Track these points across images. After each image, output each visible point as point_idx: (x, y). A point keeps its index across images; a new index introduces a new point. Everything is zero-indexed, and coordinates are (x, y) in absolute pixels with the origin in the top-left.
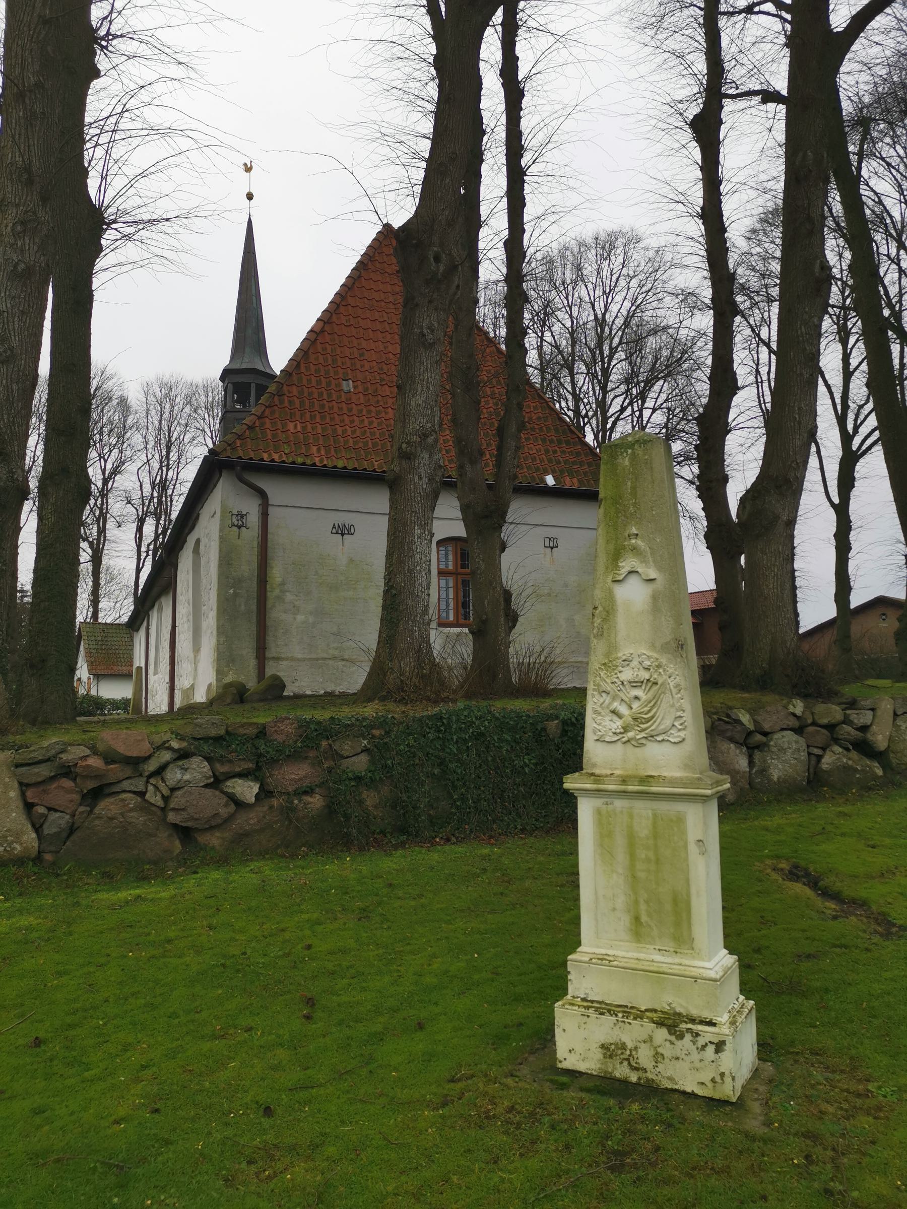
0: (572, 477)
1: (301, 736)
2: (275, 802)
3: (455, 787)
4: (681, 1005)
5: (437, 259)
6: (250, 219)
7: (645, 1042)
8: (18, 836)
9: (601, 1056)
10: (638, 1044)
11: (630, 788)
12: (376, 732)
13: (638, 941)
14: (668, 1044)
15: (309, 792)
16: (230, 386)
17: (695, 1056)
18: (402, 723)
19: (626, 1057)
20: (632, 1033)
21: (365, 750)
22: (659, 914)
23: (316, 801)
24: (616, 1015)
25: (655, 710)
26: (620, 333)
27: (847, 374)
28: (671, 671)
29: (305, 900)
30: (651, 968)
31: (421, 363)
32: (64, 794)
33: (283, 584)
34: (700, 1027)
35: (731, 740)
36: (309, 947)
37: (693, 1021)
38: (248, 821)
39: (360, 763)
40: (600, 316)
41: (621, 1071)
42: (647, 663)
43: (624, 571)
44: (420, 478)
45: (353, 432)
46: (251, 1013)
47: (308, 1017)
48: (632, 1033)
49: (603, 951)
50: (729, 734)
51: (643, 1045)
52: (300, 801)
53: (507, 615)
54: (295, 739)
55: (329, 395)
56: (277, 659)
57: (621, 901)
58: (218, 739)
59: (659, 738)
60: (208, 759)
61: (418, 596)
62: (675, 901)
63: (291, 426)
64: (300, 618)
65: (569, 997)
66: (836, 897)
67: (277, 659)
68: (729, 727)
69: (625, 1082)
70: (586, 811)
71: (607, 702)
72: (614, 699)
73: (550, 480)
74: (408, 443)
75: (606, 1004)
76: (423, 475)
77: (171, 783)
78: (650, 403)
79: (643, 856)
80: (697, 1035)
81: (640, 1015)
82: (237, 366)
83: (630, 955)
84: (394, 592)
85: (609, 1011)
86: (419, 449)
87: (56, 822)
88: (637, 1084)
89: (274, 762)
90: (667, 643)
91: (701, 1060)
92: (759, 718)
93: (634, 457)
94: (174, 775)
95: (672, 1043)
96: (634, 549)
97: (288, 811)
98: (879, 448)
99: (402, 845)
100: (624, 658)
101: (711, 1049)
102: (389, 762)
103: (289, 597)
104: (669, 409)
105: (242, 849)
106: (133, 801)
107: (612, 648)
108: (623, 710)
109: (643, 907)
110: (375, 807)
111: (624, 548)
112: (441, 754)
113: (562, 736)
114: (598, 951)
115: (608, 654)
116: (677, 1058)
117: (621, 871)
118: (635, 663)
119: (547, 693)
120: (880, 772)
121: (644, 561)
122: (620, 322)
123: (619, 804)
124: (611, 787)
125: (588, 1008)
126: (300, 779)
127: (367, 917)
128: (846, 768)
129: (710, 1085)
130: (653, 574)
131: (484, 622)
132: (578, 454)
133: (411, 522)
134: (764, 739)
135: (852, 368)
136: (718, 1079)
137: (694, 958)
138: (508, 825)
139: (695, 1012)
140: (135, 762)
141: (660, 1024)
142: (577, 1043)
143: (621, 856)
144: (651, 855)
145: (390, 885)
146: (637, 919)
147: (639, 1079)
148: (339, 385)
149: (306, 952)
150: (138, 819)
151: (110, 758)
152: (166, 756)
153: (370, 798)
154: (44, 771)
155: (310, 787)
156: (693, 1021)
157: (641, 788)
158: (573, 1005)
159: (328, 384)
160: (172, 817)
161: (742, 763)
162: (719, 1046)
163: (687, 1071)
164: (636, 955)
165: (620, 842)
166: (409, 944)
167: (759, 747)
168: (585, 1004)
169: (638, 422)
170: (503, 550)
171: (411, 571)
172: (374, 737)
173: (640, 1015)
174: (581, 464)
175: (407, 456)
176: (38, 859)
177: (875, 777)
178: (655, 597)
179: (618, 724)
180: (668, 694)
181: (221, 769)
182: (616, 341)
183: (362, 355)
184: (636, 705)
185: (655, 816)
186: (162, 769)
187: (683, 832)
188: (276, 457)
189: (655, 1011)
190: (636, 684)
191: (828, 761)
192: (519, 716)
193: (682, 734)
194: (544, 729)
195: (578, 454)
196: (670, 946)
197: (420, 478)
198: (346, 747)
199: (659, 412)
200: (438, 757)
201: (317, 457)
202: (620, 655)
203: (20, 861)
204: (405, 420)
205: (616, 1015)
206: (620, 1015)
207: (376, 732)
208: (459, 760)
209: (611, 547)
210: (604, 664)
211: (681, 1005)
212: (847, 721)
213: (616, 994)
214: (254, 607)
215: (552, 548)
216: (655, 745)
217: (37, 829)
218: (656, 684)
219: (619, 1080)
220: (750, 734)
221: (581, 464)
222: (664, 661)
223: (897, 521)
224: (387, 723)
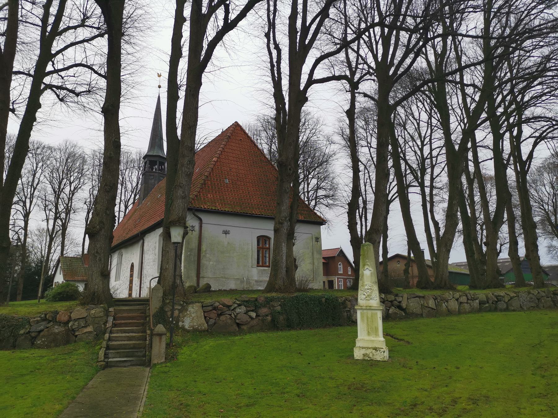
2: (260, 318)
4: (377, 346)
5: (290, 169)
6: (159, 97)
8: (204, 324)
15: (267, 316)
16: (148, 162)
20: (368, 352)
22: (372, 331)
23: (269, 318)
32: (213, 314)
33: (206, 251)
38: (254, 322)
39: (278, 308)
41: (367, 358)
45: (230, 198)
55: (221, 184)
56: (203, 277)
57: (365, 329)
58: (247, 301)
60: (245, 306)
63: (209, 195)
64: (211, 263)
66: (397, 339)
67: (203, 277)
70: (359, 313)
77: (237, 312)
81: (370, 348)
82: (151, 154)
87: (212, 321)
89: (260, 307)
94: (238, 310)
97: (263, 321)
98: (398, 199)
103: (208, 255)
105: (252, 330)
106: (228, 316)
107: (363, 282)
120: (404, 314)
123: (365, 311)
128: (395, 313)
140: (228, 307)
142: (358, 354)
143: (366, 321)
148: (223, 181)
150: (229, 321)
151: (224, 305)
152: (236, 305)
153: (281, 318)
154: (210, 308)
157: (369, 308)
159: (220, 180)
160: (237, 321)
162: (384, 352)
163: (379, 356)
165: (365, 318)
173: (370, 348)
175: (282, 224)
176: (207, 331)
177: (403, 316)
178: (371, 273)
179: (365, 297)
181: (249, 309)
183: (230, 170)
186: (235, 308)
188: (206, 207)
191: (391, 311)
196: (375, 336)
198: (275, 304)
201: (219, 207)
203: (204, 331)
212: (395, 300)
214: (196, 259)
217: (207, 323)
223: (404, 228)
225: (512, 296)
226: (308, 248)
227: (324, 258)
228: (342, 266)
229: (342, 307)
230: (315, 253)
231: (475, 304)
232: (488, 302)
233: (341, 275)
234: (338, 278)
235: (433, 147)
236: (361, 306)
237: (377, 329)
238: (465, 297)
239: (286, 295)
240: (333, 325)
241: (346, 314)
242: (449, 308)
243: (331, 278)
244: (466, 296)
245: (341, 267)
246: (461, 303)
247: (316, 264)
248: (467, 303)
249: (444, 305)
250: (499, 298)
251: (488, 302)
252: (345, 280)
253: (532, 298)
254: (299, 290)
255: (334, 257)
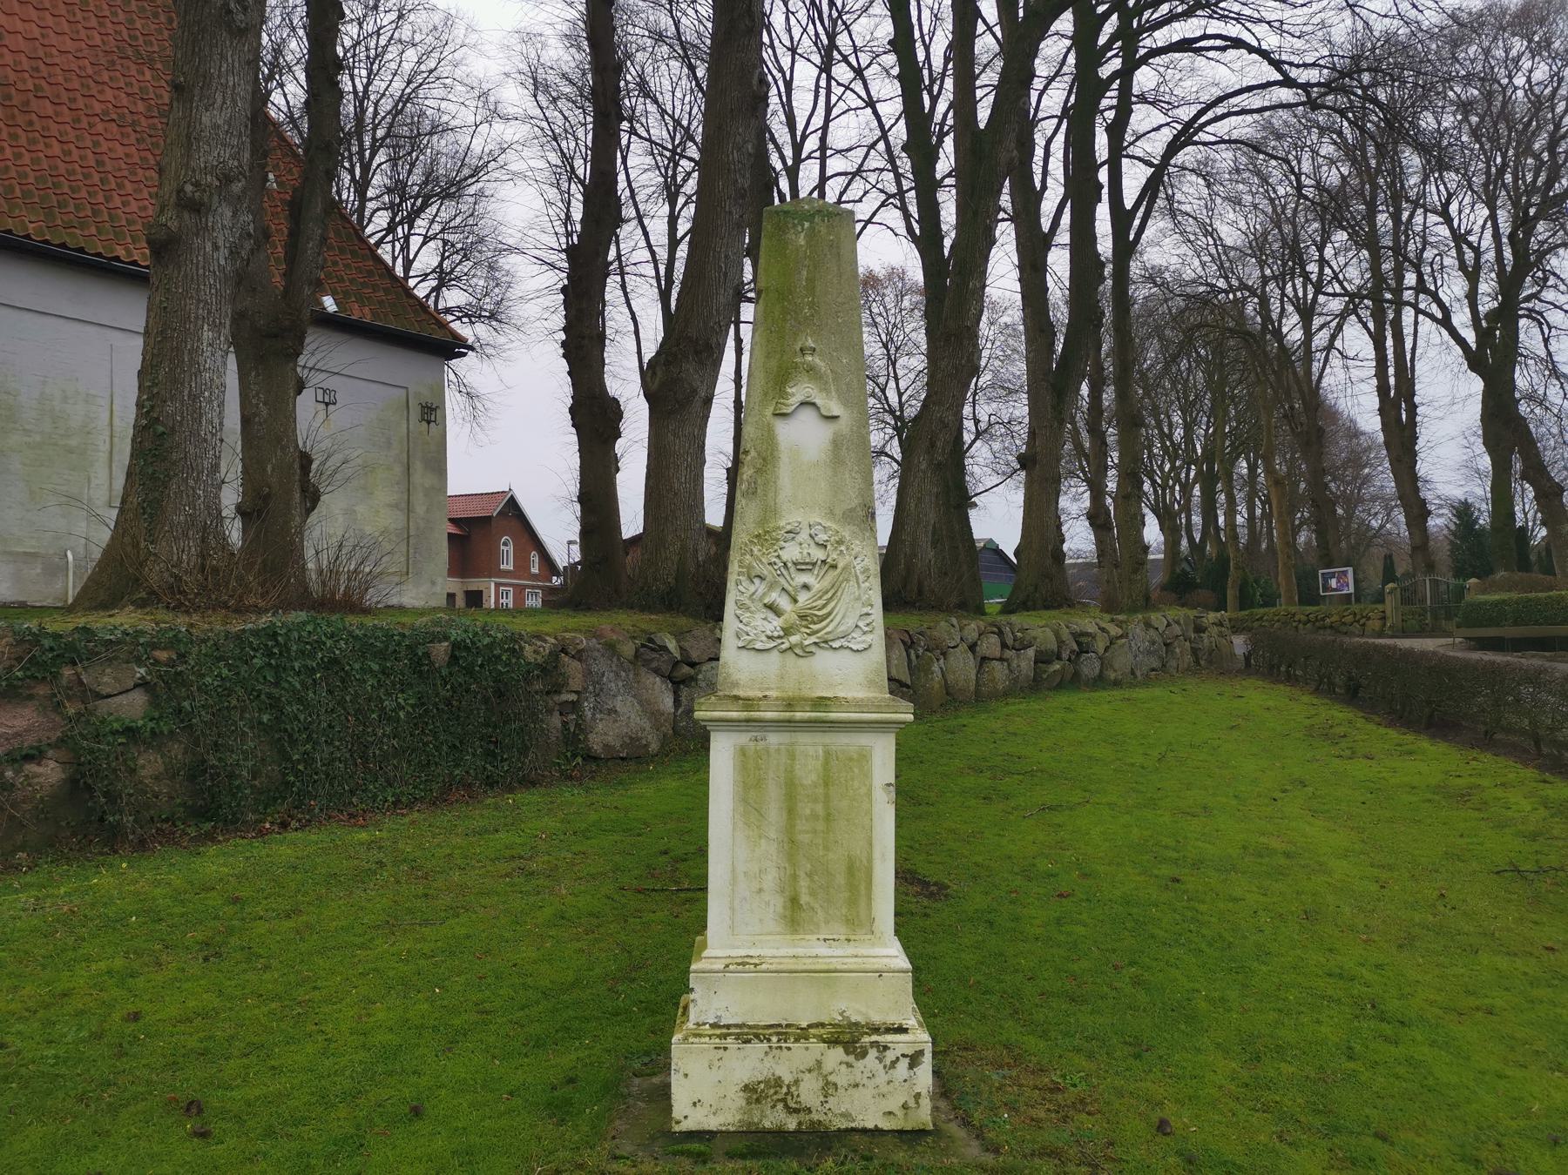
0: (362, 306)
1: (19, 659)
3: (293, 742)
4: (859, 1010)
7: (810, 1071)
9: (744, 1103)
10: (801, 1075)
11: (799, 715)
12: (163, 655)
13: (795, 932)
14: (844, 1067)
15: (35, 756)
17: (882, 1078)
18: (204, 641)
19: (780, 1097)
20: (790, 1063)
21: (142, 684)
23: (49, 773)
24: (769, 1040)
25: (832, 604)
26: (388, 119)
27: (674, 243)
28: (857, 549)
29: (84, 940)
30: (818, 967)
31: (223, 57)
34: (889, 1037)
35: (657, 671)
36: (136, 1017)
37: (876, 1030)
39: (132, 706)
40: (360, 88)
41: (774, 1118)
42: (822, 537)
43: (794, 401)
44: (216, 247)
46: (79, 1147)
47: (203, 1135)
48: (790, 1063)
49: (743, 952)
50: (654, 665)
51: (807, 1076)
52: (17, 772)
53: (304, 491)
54: (7, 663)
57: (770, 880)
59: (836, 644)
61: (205, 440)
62: (851, 870)
65: (690, 1025)
68: (655, 655)
69: (779, 1133)
70: (723, 753)
71: (760, 591)
72: (771, 587)
73: (329, 304)
74: (197, 185)
75: (750, 1027)
76: (221, 243)
78: (421, 224)
79: (808, 812)
80: (886, 1048)
81: (802, 1034)
83: (782, 952)
84: (161, 429)
85: (757, 1036)
86: (216, 198)
88: (798, 1132)
90: (851, 510)
91: (889, 1082)
92: (686, 645)
93: (812, 234)
95: (849, 1065)
96: (811, 370)
99: (210, 837)
100: (789, 528)
101: (904, 1063)
102: (186, 704)
104: (445, 242)
108: (784, 603)
109: (804, 883)
110: (157, 778)
111: (796, 366)
112: (274, 691)
113: (449, 665)
114: (734, 953)
115: (763, 521)
116: (856, 1086)
117: (773, 835)
118: (803, 536)
119: (366, 611)
121: (825, 389)
122: (386, 104)
123: (774, 739)
124: (769, 715)
125: (725, 1036)
126: (17, 735)
127: (218, 955)
129: (900, 1113)
130: (835, 408)
131: (266, 498)
132: (370, 274)
133: (197, 318)
134: (692, 671)
135: (679, 235)
136: (912, 1103)
137: (873, 945)
138: (375, 797)
139: (877, 1018)
141: (832, 1042)
142: (705, 1089)
144: (819, 808)
145: (236, 900)
146: (794, 901)
147: (800, 1123)
149: (131, 1027)
153: (149, 764)
155: (38, 748)
156: (876, 1030)
157: (814, 716)
158: (700, 1036)
161: (667, 702)
164: (791, 952)
165: (774, 794)
166: (315, 988)
167: (689, 681)
168: (718, 1032)
169: (402, 249)
170: (300, 393)
171: (194, 397)
172: (157, 662)
173: (802, 1034)
174: (375, 288)
175: (196, 208)
178: (836, 443)
179: (774, 625)
180: (853, 583)
182: (380, 133)
184: (803, 597)
185: (827, 754)
187: (867, 775)
189: (822, 1025)
190: (804, 566)
192: (389, 636)
193: (868, 638)
194: (427, 655)
195: (370, 274)
196: (840, 931)
197: (216, 247)
198: (107, 680)
199: (432, 244)
200: (269, 696)
202: (782, 523)
204: (190, 144)
205: (769, 1040)
206: (774, 1039)
207: (163, 655)
208: (300, 701)
209: (774, 363)
210: (758, 536)
211: (860, 1012)
213: (763, 1009)
215: (327, 404)
216: (829, 654)
218: (834, 567)
219: (770, 1132)
220: (676, 664)
221: (375, 288)
222: (847, 535)
224: (179, 641)
225: (1113, 633)
226: (389, 445)
227: (451, 520)
228: (511, 548)
229: (538, 686)
230: (418, 466)
231: (1023, 664)
232: (1059, 658)
233: (506, 574)
234: (498, 585)
235: (829, 173)
236: (748, 703)
237: (858, 876)
238: (994, 639)
239: (212, 625)
240: (491, 783)
241: (556, 720)
242: (950, 677)
243: (475, 584)
244: (1000, 633)
245: (507, 551)
246: (984, 659)
247: (420, 509)
248: (1001, 659)
249: (936, 668)
250: (1083, 639)
251: (1059, 658)
252: (519, 590)
253: (1153, 643)
254: (304, 600)
255: (490, 518)
